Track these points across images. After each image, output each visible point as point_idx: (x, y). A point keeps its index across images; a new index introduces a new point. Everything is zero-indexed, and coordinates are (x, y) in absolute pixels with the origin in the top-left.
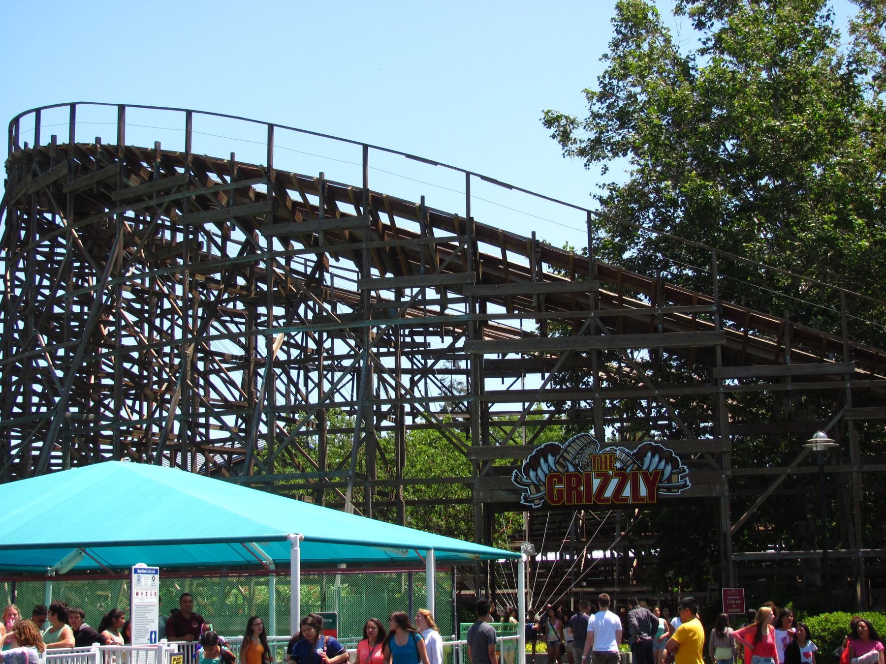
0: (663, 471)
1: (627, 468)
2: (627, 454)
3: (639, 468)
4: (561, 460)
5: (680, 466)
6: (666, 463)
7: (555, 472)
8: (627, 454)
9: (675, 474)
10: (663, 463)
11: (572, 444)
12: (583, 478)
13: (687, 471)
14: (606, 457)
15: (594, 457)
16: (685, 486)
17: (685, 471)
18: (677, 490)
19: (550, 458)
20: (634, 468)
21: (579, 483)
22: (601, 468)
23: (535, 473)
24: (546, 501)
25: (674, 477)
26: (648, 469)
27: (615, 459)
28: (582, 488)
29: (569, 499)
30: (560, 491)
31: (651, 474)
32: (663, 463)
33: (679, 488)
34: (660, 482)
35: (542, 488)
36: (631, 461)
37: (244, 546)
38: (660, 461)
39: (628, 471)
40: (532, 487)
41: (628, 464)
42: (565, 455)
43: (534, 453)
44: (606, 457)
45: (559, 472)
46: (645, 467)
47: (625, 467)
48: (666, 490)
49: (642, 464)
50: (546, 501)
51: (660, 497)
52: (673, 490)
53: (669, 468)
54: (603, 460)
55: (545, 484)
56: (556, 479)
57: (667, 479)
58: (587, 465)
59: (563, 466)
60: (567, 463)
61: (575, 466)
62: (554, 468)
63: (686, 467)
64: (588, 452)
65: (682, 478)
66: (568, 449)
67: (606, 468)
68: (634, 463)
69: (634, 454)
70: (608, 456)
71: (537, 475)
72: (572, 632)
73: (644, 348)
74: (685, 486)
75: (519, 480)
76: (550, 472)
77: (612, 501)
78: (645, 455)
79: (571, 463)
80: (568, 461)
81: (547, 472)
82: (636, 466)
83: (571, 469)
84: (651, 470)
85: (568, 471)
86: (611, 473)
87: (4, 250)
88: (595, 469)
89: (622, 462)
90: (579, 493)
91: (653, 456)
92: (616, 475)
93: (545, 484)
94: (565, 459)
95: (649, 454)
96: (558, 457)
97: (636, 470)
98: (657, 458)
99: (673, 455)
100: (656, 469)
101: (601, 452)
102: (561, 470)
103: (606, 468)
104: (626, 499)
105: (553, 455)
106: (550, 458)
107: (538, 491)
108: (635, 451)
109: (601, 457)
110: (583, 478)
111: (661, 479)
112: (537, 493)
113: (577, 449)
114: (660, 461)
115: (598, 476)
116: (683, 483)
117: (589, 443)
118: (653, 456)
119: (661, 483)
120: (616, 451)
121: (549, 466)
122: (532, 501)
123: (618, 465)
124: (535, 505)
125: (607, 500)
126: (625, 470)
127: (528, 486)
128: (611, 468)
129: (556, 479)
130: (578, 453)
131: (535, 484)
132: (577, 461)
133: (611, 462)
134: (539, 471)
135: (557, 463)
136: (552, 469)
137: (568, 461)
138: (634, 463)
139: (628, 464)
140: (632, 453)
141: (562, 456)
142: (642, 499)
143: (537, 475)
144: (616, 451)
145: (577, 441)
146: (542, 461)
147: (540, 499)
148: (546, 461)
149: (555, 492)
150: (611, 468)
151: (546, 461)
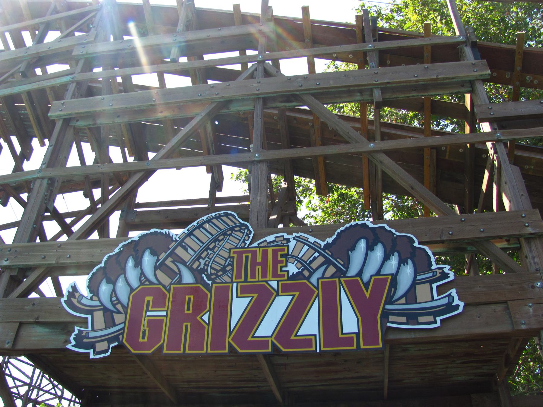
0: (395, 278)
1: (311, 274)
2: (313, 247)
3: (341, 273)
4: (168, 262)
5: (434, 266)
6: (402, 261)
7: (151, 283)
8: (313, 247)
9: (422, 282)
10: (394, 261)
11: (196, 233)
12: (211, 299)
13: (452, 276)
14: (265, 253)
15: (240, 254)
16: (449, 307)
17: (445, 276)
18: (430, 318)
19: (148, 260)
20: (328, 275)
21: (199, 307)
22: (253, 276)
23: (111, 286)
24: (121, 346)
25: (422, 291)
26: (360, 274)
27: (286, 256)
28: (206, 318)
29: (174, 342)
30: (156, 324)
31: (367, 285)
32: (394, 261)
33: (435, 312)
34: (390, 300)
35: (119, 318)
36: (321, 260)
37: (18, 322)
38: (386, 258)
39: (314, 280)
40: (99, 316)
41: (314, 265)
42: (180, 251)
43: (117, 250)
44: (265, 253)
45: (160, 283)
46: (353, 270)
47: (306, 273)
48: (404, 319)
49: (347, 265)
50: (121, 346)
51: (392, 336)
52: (421, 319)
53: (408, 271)
54: (259, 259)
55: (125, 308)
56: (150, 298)
57: (405, 295)
58: (224, 270)
59: (171, 273)
60: (181, 267)
61: (197, 273)
62: (151, 277)
63: (447, 268)
64: (228, 246)
65: (441, 290)
66: (188, 241)
67: (264, 275)
68: (328, 263)
69: (328, 246)
70: (270, 251)
71: (114, 291)
72: (248, 179)
73: (333, 113)
74: (449, 307)
75: (74, 301)
76: (141, 283)
77: (273, 343)
78: (353, 248)
79: (190, 268)
80: (184, 263)
81: (135, 283)
82: (331, 270)
83: (188, 278)
84: (366, 276)
85: (180, 282)
86: (274, 284)
87: (201, 268)
88: (239, 276)
89: (300, 260)
90: (198, 328)
91: (370, 248)
92: (286, 289)
93: (125, 308)
94: (179, 260)
95: (362, 245)
96: (163, 256)
97: (332, 277)
98: (379, 252)
99: (416, 245)
100: (378, 273)
101: (255, 244)
102: (165, 280)
103: (264, 275)
104: (307, 341)
105: (154, 253)
106: (148, 260)
107: (110, 322)
108: (330, 240)
109: (254, 253)
110: (211, 299)
111: (390, 300)
112: (107, 327)
113: (204, 239)
114: (386, 258)
115: (244, 291)
116: (445, 301)
117: (232, 229)
118: (370, 248)
119: (392, 303)
120: (288, 240)
121: (142, 273)
122: (92, 346)
123: (292, 269)
124: (95, 353)
125: (262, 342)
126: (308, 279)
127: (91, 312)
128: (275, 275)
129: (150, 298)
130: (207, 248)
131: (105, 310)
132: (202, 262)
133: (276, 262)
134: (121, 284)
135: (159, 266)
136: (147, 279)
137: (184, 263)
138: (328, 263)
139: (314, 265)
140: (323, 244)
141: (172, 254)
142: (348, 340)
143: (114, 291)
144: (288, 240)
145: (207, 226)
146: (130, 264)
147: (110, 341)
148: (138, 264)
149: (144, 326)
150: (275, 275)
151: (138, 264)
